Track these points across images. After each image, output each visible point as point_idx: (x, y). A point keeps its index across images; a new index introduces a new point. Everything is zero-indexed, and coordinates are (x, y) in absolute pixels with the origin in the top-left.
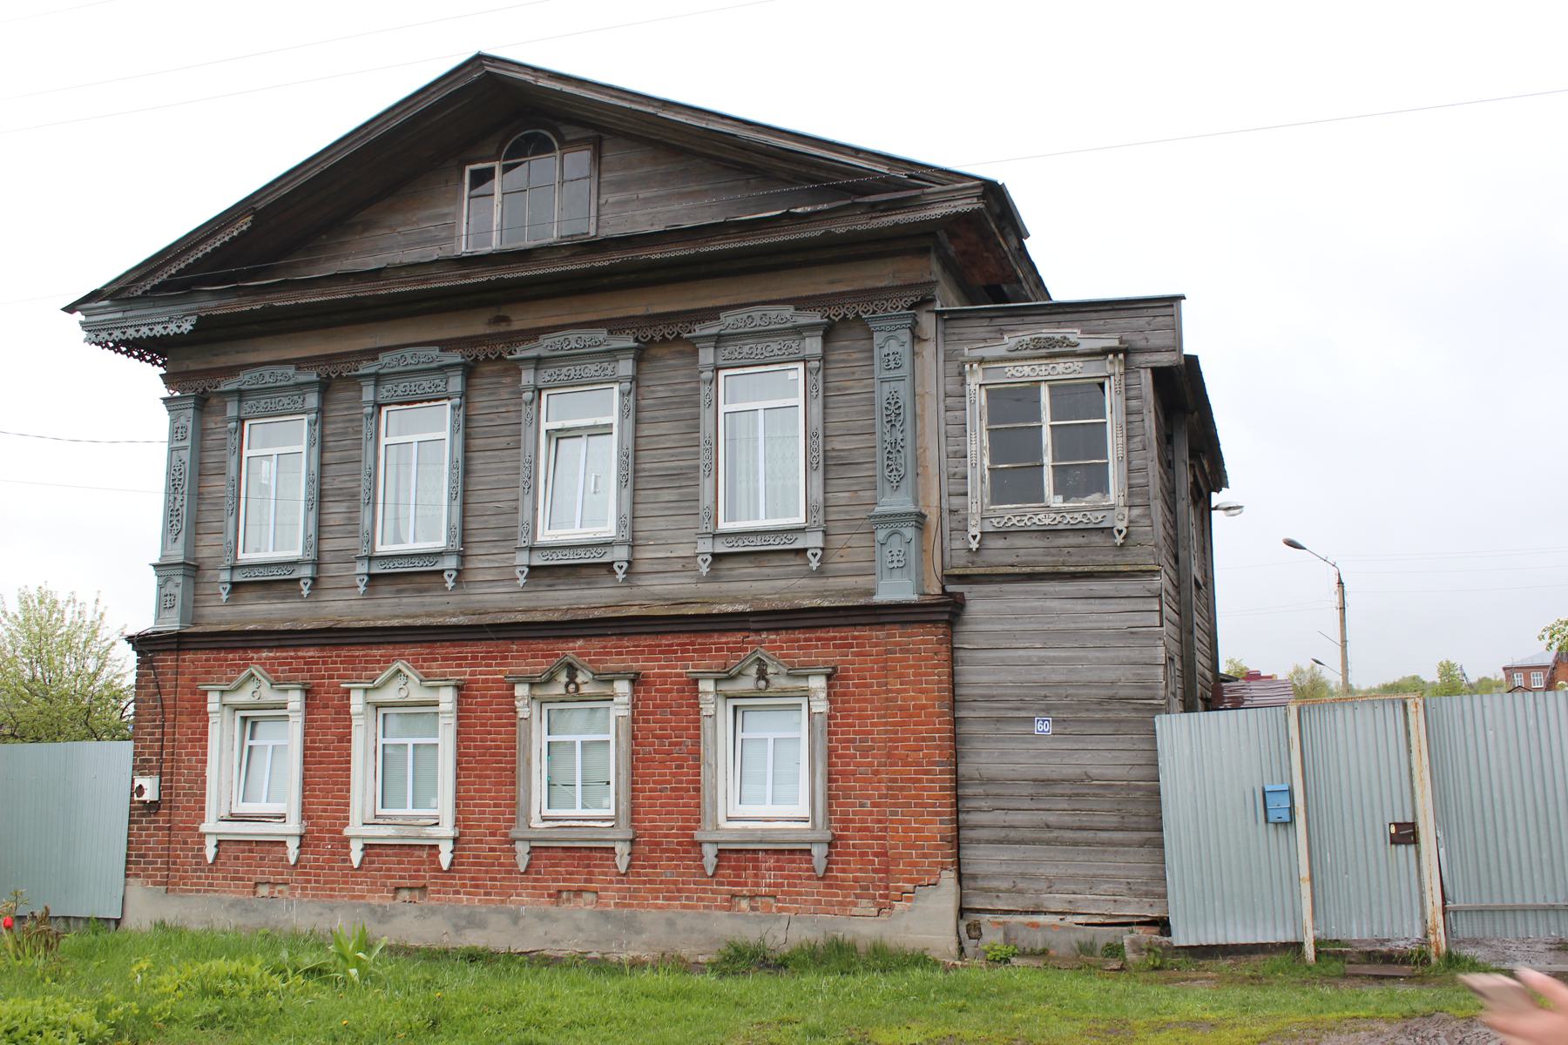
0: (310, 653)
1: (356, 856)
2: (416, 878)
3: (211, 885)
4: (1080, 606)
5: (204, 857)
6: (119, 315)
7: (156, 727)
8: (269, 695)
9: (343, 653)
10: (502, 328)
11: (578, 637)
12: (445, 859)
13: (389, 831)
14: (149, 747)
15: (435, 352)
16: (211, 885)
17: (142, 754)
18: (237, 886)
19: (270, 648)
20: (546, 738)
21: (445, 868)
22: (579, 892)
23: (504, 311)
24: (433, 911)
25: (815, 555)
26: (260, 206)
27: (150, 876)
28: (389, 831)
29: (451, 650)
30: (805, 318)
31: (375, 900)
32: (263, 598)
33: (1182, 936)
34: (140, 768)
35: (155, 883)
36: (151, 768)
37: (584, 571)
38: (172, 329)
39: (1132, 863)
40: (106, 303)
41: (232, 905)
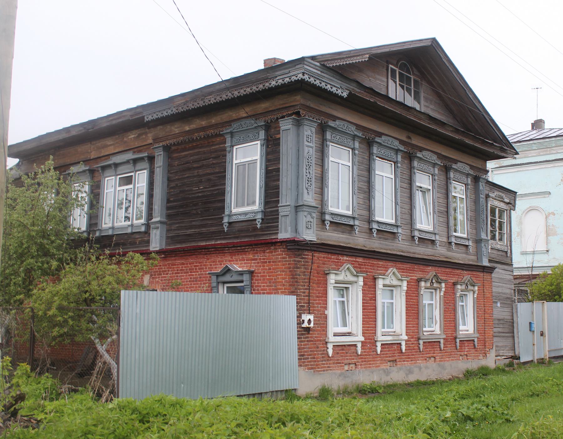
0: (360, 260)
1: (379, 349)
2: (392, 356)
3: (329, 367)
4: (503, 272)
5: (376, 351)
6: (319, 73)
7: (306, 289)
8: (351, 278)
9: (371, 262)
10: (409, 141)
11: (430, 265)
12: (404, 348)
13: (390, 338)
14: (304, 299)
15: (353, 128)
16: (329, 367)
17: (300, 303)
18: (338, 367)
19: (347, 255)
20: (394, 301)
21: (330, 356)
22: (430, 358)
23: (411, 135)
24: (400, 369)
25: (259, 222)
26: (374, 52)
27: (306, 365)
28: (390, 338)
29: (400, 265)
30: (471, 172)
31: (383, 367)
32: (335, 230)
33: (523, 360)
34: (301, 310)
35: (309, 369)
36: (305, 310)
37: (426, 241)
38: (339, 92)
39: (509, 342)
40: (318, 64)
41: (340, 375)
